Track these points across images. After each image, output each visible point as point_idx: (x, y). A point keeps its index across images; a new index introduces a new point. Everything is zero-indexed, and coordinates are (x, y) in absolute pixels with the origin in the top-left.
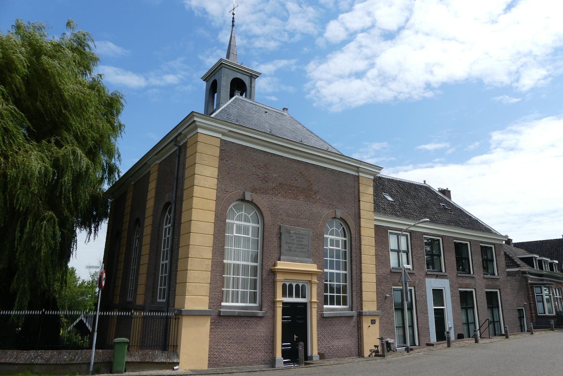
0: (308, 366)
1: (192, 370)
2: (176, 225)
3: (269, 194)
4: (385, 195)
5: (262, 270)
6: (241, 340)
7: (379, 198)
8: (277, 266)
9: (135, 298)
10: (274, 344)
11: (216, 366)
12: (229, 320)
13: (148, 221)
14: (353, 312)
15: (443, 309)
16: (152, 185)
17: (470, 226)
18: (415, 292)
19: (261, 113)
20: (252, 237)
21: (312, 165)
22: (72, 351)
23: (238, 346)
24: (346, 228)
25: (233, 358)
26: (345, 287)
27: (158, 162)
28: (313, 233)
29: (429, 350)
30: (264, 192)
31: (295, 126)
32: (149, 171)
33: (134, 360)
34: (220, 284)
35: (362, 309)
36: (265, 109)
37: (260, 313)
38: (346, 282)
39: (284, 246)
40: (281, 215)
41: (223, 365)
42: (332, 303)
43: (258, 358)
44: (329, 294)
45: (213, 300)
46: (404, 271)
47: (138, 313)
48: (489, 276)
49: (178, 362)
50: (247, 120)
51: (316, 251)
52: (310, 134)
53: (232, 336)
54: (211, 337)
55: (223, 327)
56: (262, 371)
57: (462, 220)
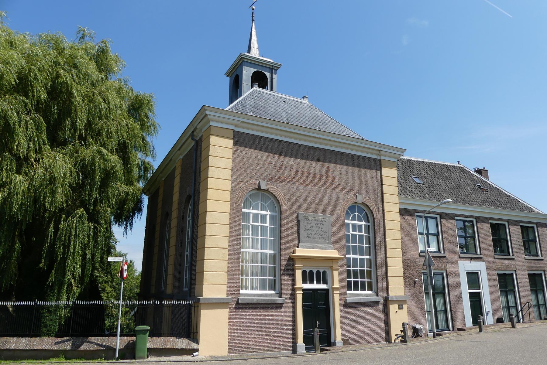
0: (324, 352)
1: (211, 357)
2: (195, 217)
3: (285, 182)
4: (413, 178)
5: (280, 257)
6: (261, 326)
7: (407, 181)
8: (295, 253)
9: (166, 288)
10: (295, 331)
11: (237, 352)
12: (248, 307)
13: (174, 214)
14: (379, 297)
15: (479, 293)
16: (177, 180)
17: (508, 206)
18: (447, 275)
19: (279, 103)
20: (269, 225)
21: (330, 151)
22: (100, 338)
23: (258, 333)
24: (370, 214)
25: (254, 344)
26: (369, 272)
27: (181, 157)
28: (333, 219)
29: (459, 335)
30: (281, 180)
31: (314, 113)
32: (174, 166)
33: (156, 347)
34: (237, 272)
35: (388, 294)
36: (284, 99)
37: (279, 300)
38: (370, 267)
39: (303, 233)
40: (298, 202)
41: (243, 352)
42: (356, 289)
43: (279, 344)
44: (359, 280)
45: (231, 288)
46: (428, 254)
47: (159, 302)
48: (531, 257)
49: (198, 348)
50: (264, 111)
51: (336, 237)
52: (331, 120)
53: (252, 322)
54: (231, 324)
55: (242, 314)
56: (277, 357)
57: (499, 199)
